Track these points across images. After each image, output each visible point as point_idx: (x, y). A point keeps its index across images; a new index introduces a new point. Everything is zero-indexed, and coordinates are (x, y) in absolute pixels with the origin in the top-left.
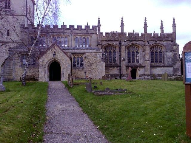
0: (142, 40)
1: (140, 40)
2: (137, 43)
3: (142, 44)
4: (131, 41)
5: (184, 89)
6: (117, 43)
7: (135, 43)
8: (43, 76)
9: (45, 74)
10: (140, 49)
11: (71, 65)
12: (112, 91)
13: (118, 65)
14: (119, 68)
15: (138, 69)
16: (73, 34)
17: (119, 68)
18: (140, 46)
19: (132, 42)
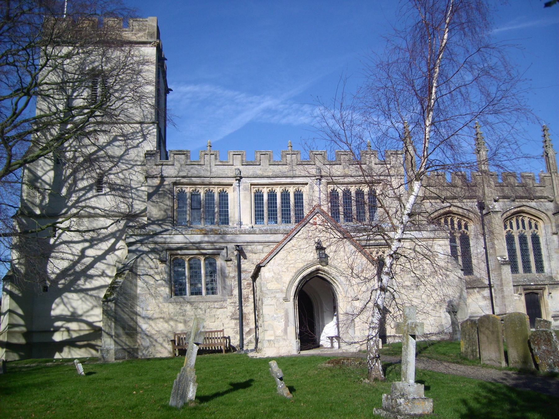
0: (545, 194)
1: (538, 194)
2: (533, 204)
3: (548, 210)
4: (514, 201)
5: (166, 276)
6: (473, 204)
7: (524, 206)
8: (279, 332)
9: (287, 325)
10: (541, 224)
11: (268, 262)
12: (32, 83)
13: (483, 283)
14: (486, 292)
15: (546, 293)
16: (324, 181)
17: (486, 292)
18: (543, 216)
19: (517, 204)
